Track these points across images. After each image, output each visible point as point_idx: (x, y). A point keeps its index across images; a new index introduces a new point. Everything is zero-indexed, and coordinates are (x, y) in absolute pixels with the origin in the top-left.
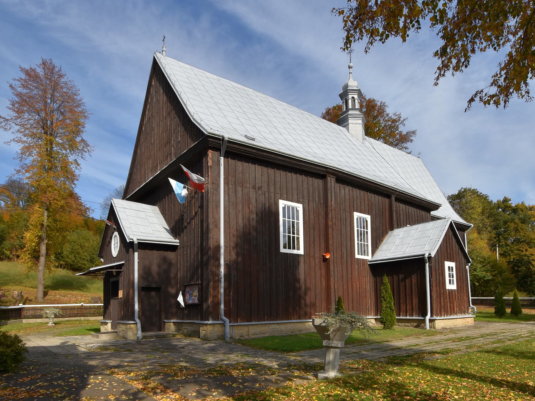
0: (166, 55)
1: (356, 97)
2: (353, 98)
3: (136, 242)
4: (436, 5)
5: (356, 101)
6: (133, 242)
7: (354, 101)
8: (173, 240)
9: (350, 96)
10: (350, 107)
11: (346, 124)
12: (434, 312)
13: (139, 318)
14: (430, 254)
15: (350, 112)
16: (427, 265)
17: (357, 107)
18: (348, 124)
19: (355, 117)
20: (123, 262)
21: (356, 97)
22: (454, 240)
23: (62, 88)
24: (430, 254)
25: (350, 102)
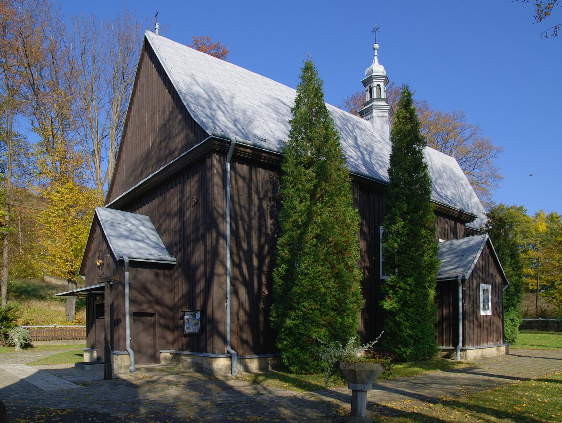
0: (159, 34)
1: (382, 84)
2: (378, 85)
3: (127, 260)
4: (412, 127)
5: (382, 89)
6: (123, 261)
7: (380, 89)
8: (169, 258)
9: (375, 84)
10: (375, 96)
11: (369, 116)
12: (467, 341)
13: (132, 348)
14: (464, 276)
15: (375, 103)
16: (460, 288)
17: (383, 97)
18: (373, 117)
19: (380, 108)
20: (104, 285)
21: (382, 84)
22: (155, 71)
23: (525, 251)
24: (464, 276)
25: (375, 90)
